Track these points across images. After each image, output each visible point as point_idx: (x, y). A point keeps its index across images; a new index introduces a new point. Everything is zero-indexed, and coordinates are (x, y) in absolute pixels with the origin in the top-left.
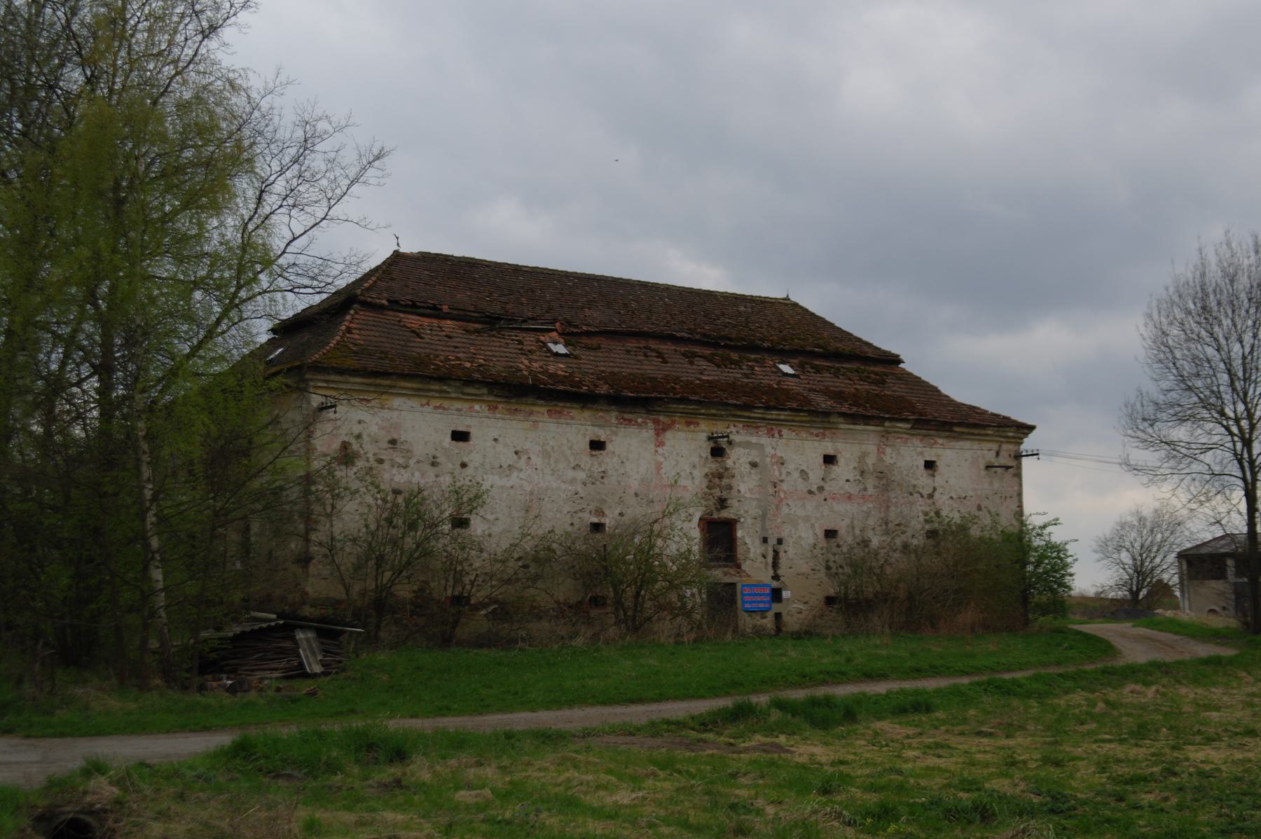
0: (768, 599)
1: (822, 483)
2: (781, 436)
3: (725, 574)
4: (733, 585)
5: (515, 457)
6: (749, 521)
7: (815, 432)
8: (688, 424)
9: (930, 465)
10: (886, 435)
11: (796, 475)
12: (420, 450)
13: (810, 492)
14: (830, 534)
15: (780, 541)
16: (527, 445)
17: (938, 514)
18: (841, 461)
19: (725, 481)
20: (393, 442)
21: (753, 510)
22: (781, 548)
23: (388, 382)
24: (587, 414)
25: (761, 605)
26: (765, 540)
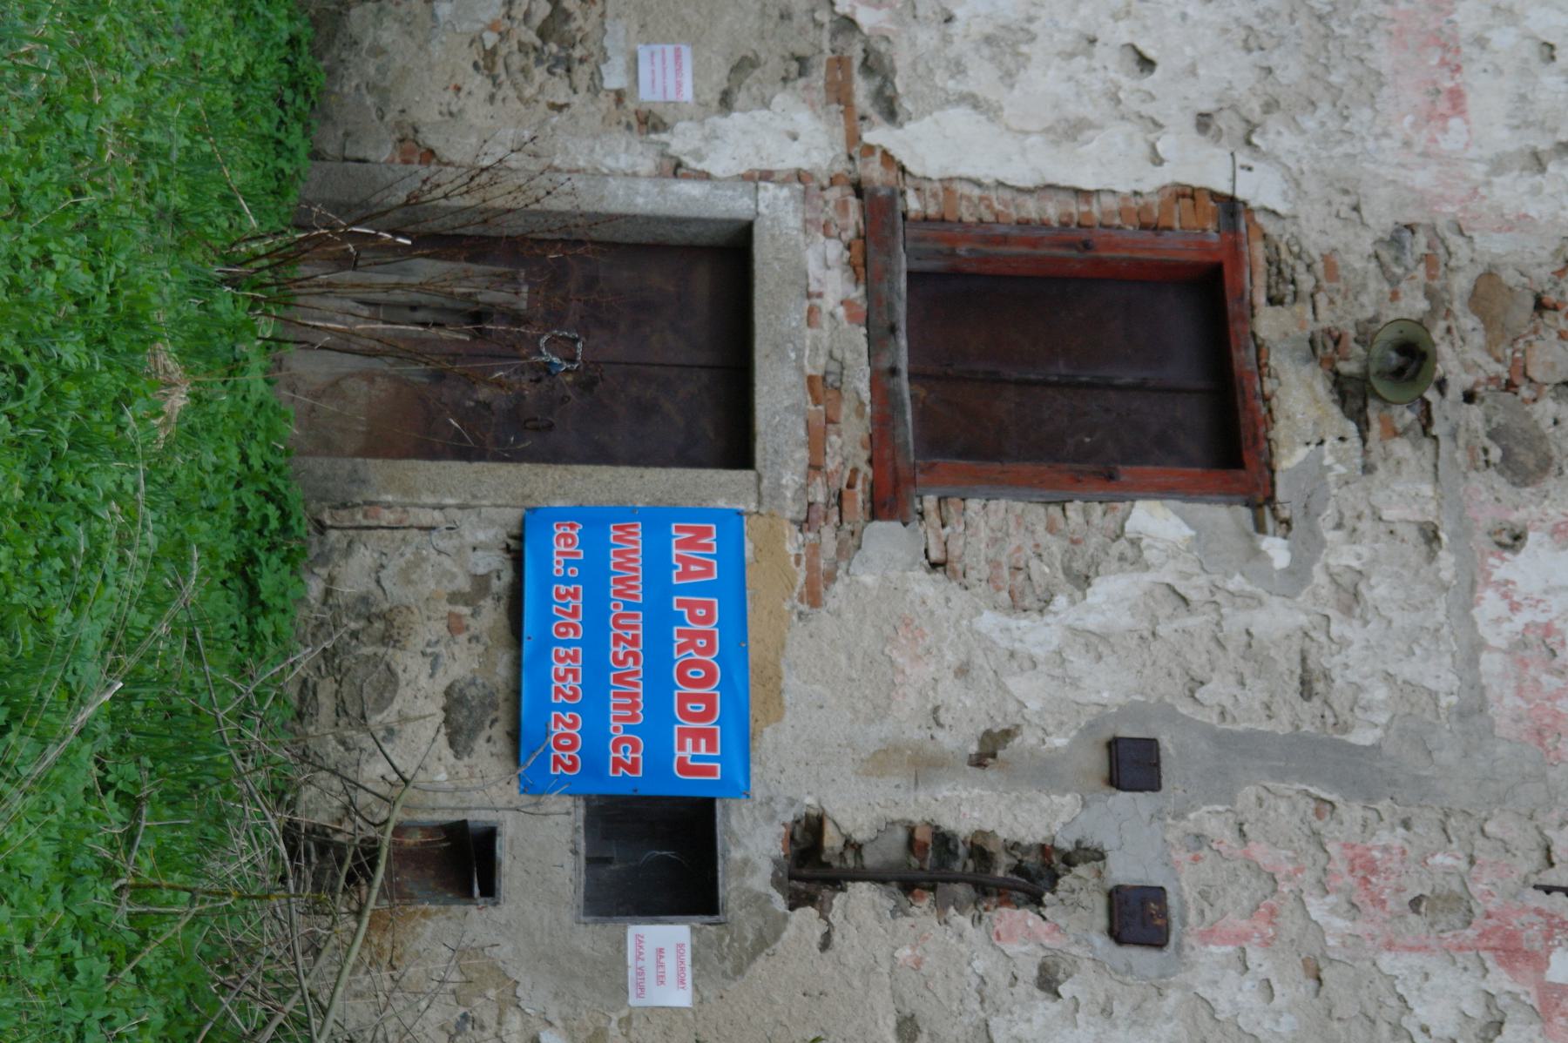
0: (627, 765)
3: (822, 388)
4: (737, 450)
6: (1277, 620)
15: (1138, 918)
21: (1384, 665)
22: (1072, 923)
25: (563, 672)
26: (1132, 764)
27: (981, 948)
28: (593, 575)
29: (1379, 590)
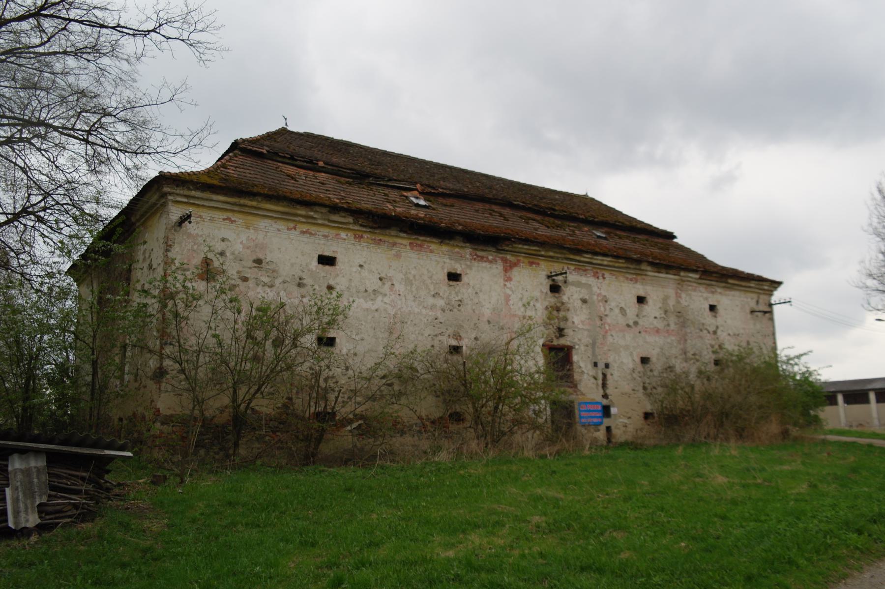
0: (600, 414)
1: (636, 319)
2: (604, 278)
5: (380, 283)
6: (583, 348)
7: (630, 276)
8: (531, 264)
9: (712, 308)
10: (681, 282)
11: (617, 311)
12: (285, 271)
13: (628, 326)
14: (645, 360)
16: (391, 273)
17: (720, 347)
18: (650, 301)
19: (562, 314)
20: (258, 262)
21: (586, 340)
22: (608, 372)
23: (254, 203)
24: (445, 248)
26: (595, 364)
27: (610, 382)
28: (586, 418)
29: (579, 337)
